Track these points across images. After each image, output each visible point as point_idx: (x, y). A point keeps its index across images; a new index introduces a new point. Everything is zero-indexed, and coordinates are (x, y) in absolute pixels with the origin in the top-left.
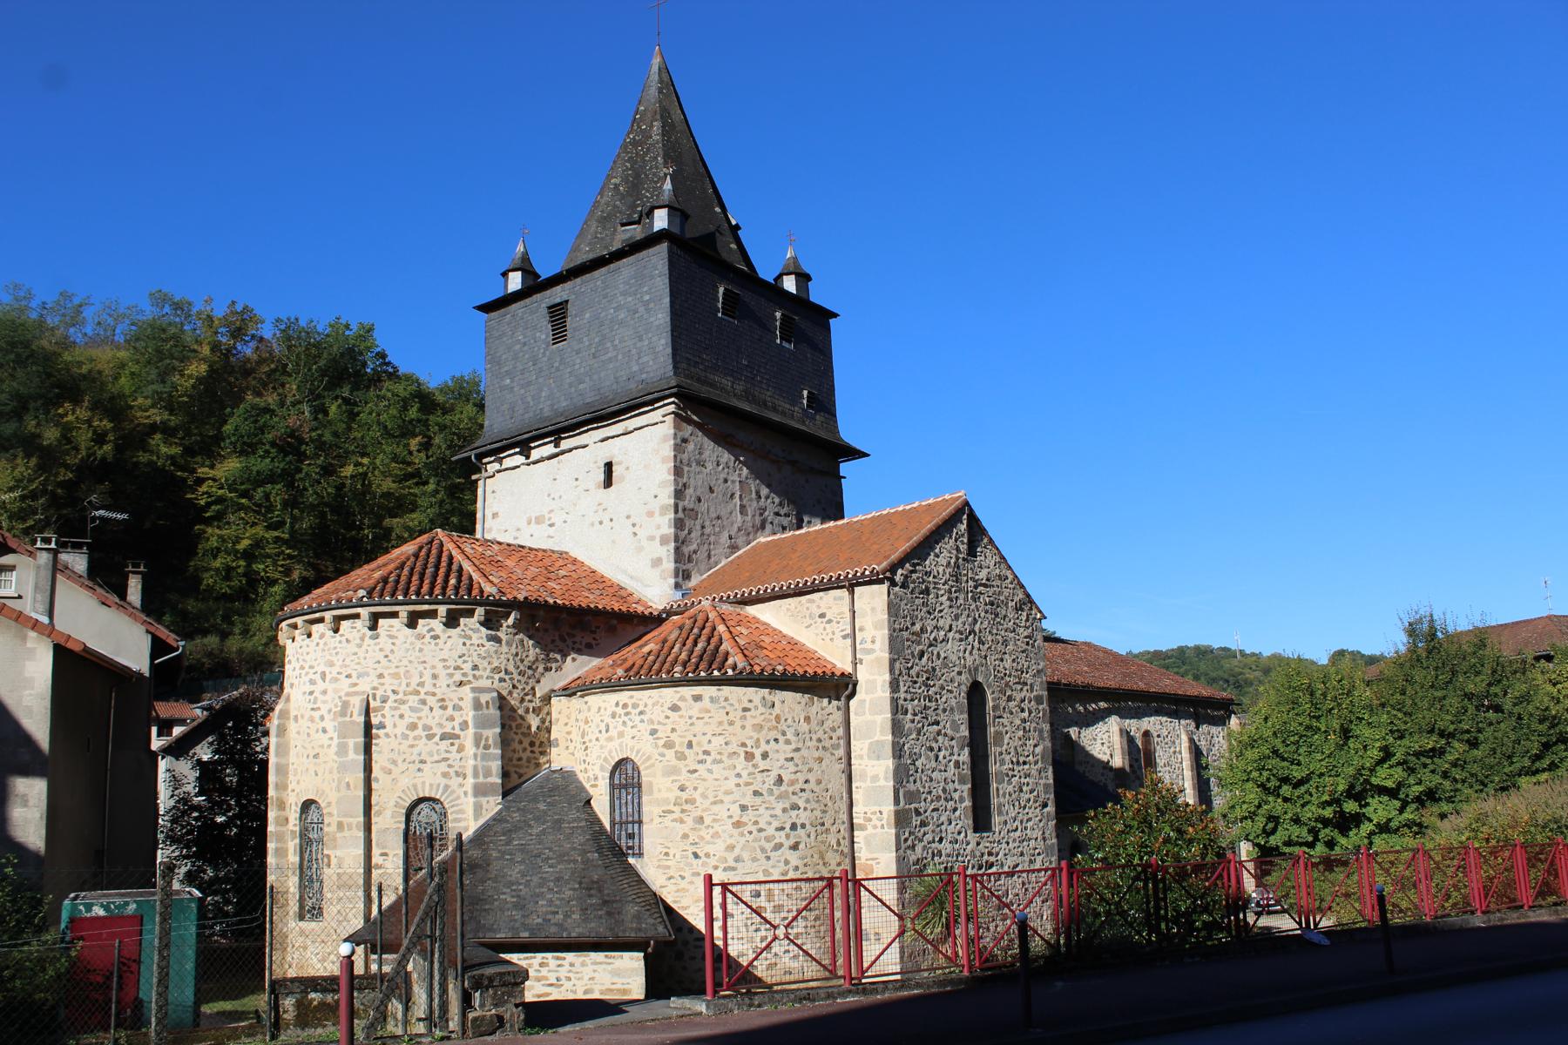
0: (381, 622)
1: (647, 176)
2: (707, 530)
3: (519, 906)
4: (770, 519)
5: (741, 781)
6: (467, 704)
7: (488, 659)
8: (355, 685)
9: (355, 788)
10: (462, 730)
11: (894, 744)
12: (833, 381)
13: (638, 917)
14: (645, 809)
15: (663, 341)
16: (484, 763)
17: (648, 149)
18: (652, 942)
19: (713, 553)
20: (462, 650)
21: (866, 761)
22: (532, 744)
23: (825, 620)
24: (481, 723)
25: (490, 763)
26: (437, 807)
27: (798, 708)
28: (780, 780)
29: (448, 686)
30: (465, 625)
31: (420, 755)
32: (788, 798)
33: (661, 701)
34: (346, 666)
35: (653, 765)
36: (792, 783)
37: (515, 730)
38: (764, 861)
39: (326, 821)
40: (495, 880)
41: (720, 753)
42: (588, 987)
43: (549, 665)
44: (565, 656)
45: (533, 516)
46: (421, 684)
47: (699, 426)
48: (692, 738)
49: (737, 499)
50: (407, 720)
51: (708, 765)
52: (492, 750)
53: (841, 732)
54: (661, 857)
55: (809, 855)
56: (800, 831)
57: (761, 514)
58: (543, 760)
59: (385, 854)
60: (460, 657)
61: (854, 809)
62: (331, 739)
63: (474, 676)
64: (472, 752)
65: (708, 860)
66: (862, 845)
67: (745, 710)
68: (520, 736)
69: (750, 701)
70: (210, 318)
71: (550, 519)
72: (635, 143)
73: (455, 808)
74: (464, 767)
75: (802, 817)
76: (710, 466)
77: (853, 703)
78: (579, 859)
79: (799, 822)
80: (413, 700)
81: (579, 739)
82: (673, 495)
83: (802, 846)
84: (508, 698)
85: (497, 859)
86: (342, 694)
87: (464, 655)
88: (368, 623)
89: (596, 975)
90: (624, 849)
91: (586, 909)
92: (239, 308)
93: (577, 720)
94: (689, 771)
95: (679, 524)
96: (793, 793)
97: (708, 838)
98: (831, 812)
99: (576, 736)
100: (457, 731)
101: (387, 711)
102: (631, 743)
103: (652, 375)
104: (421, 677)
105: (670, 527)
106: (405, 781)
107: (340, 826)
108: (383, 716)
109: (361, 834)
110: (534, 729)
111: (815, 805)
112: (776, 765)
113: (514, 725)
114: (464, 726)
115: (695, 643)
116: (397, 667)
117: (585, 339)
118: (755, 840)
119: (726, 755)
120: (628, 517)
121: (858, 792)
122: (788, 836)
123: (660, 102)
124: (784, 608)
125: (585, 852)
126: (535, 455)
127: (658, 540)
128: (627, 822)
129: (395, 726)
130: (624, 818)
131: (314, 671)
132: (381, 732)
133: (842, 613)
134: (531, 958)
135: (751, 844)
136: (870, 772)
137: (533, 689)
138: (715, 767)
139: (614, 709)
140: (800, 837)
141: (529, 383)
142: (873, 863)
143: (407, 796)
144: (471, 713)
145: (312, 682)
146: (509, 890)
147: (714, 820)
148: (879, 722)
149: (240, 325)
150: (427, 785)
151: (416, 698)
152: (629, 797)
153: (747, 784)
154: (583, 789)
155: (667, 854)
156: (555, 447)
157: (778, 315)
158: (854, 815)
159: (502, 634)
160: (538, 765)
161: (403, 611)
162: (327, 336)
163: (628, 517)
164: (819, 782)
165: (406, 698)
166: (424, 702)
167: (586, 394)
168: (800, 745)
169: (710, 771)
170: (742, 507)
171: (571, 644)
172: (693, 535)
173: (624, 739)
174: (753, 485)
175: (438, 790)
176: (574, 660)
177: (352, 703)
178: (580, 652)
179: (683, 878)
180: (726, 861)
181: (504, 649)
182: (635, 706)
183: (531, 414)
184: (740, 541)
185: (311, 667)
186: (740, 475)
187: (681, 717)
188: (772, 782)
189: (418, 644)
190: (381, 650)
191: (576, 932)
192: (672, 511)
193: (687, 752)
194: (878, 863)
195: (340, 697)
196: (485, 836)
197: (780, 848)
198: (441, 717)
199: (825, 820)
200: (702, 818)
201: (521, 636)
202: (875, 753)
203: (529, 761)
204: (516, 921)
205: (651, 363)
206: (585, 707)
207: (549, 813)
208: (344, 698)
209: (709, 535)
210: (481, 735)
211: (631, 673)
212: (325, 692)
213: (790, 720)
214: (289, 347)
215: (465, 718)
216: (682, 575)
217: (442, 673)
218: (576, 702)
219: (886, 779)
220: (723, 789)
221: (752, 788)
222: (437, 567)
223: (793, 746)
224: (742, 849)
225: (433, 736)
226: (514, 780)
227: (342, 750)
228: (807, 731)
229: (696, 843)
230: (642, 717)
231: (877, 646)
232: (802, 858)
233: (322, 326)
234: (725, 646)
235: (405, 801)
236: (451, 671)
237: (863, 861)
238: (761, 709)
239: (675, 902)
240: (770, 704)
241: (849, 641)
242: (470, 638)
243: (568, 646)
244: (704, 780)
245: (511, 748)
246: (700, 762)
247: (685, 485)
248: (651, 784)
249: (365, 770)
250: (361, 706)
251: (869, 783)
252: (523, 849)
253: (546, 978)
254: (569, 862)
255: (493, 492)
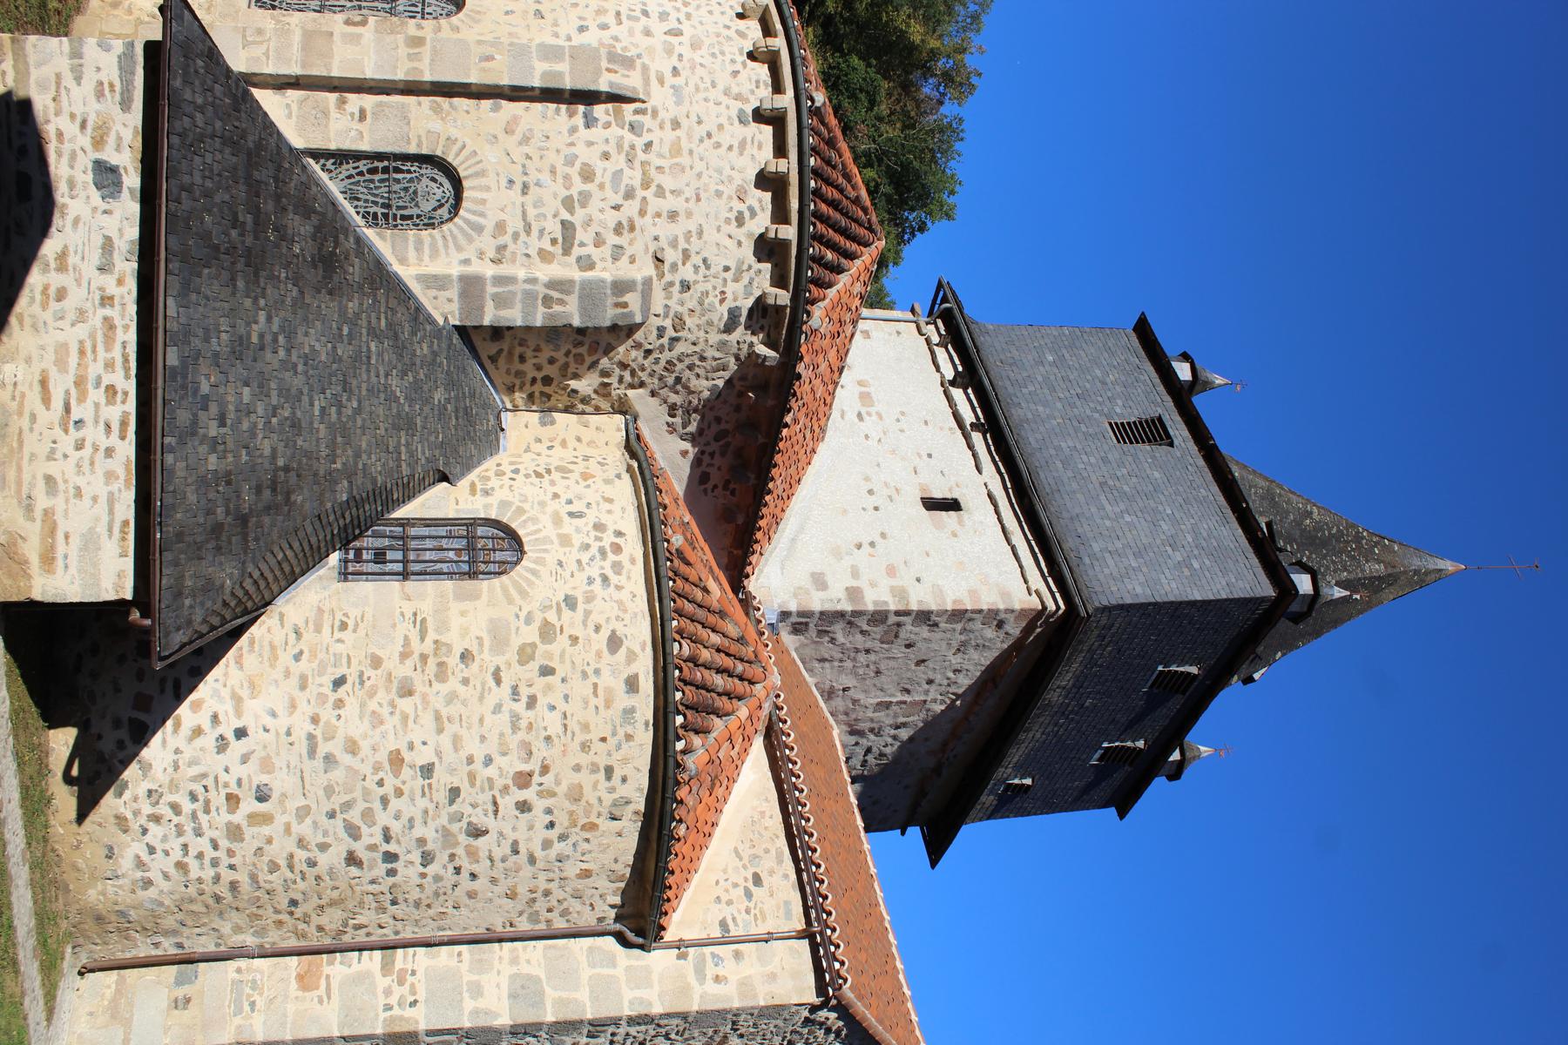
0: (768, 130)
1: (1324, 557)
2: (862, 658)
3: (240, 349)
4: (863, 742)
5: (478, 765)
6: (624, 270)
7: (698, 309)
8: (661, 82)
9: (483, 70)
10: (579, 259)
11: (538, 1026)
12: (1035, 814)
13: (209, 587)
14: (430, 587)
15: (1139, 590)
16: (519, 296)
17: (1353, 558)
18: (148, 622)
19: (827, 665)
20: (717, 263)
21: (508, 970)
22: (547, 381)
23: (750, 885)
24: (590, 294)
25: (519, 306)
26: (444, 212)
27: (607, 859)
28: (477, 832)
29: (656, 239)
30: (760, 271)
31: (538, 184)
32: (444, 848)
33: (627, 617)
34: (693, 68)
35: (510, 601)
36: (472, 854)
37: (574, 351)
38: (327, 807)
39: (424, 23)
40: (299, 303)
41: (530, 726)
42: (61, 486)
43: (680, 412)
44: (693, 439)
45: (871, 390)
46: (660, 192)
47: (1018, 645)
48: (560, 673)
49: (900, 697)
50: (599, 166)
51: (510, 705)
52: (541, 310)
53: (560, 924)
54: (339, 616)
55: (337, 884)
56: (382, 868)
57: (872, 730)
58: (519, 397)
59: (362, 115)
60: (705, 261)
61: (421, 951)
62: (569, 39)
63: (671, 284)
64: (538, 274)
65: (330, 704)
66: (356, 967)
67: (609, 771)
68: (562, 360)
69: (624, 780)
70: (964, 50)
71: (869, 414)
72: (1358, 538)
73: (440, 242)
74: (514, 261)
75: (409, 871)
76: (956, 660)
77: (610, 941)
78: (338, 466)
79: (398, 865)
80: (633, 177)
81: (555, 462)
82: (924, 608)
83: (354, 871)
84: (630, 342)
85: (343, 312)
86: (646, 60)
87: (708, 267)
88: (767, 105)
89: (87, 501)
90: (357, 544)
91: (229, 483)
92: (974, 80)
93: (586, 458)
94: (498, 670)
95: (879, 617)
96: (452, 857)
97: (373, 705)
98: (416, 914)
99: (558, 456)
100: (577, 251)
101: (615, 131)
102: (551, 560)
103: (1091, 572)
104: (673, 192)
105: (875, 603)
106: (491, 156)
107: (418, 42)
108: (607, 125)
109: (400, 75)
110: (573, 384)
111: (429, 890)
112: (507, 825)
113: (583, 350)
114: (586, 263)
115: (719, 671)
116: (691, 152)
117: (1124, 471)
118: (366, 793)
119: (528, 738)
120: (883, 535)
121: (450, 955)
122: (372, 848)
123: (1405, 572)
124: (764, 806)
125: (350, 474)
126: (957, 393)
127: (855, 584)
128: (405, 550)
129: (590, 144)
130: (413, 544)
131: (683, 18)
132: (579, 120)
133: (764, 919)
134: (127, 370)
135: (360, 784)
136: (487, 981)
137: (642, 385)
138: (505, 717)
139: (611, 529)
140: (371, 868)
141: (1053, 390)
142: (322, 990)
143: (467, 159)
144: (608, 276)
145: (663, 16)
146: (275, 328)
147: (405, 718)
148: (577, 995)
149: (958, 82)
150: (484, 195)
151: (637, 183)
152: (451, 554)
153: (472, 777)
154: (468, 467)
155: (344, 626)
156: (972, 425)
157: (1141, 744)
158: (411, 950)
159: (740, 333)
160: (511, 390)
161: (788, 166)
162: (944, 171)
163: (883, 535)
164: (471, 895)
165: (637, 164)
166: (629, 195)
167: (1048, 475)
168: (540, 864)
169: (497, 709)
170: (888, 705)
171: (709, 449)
172: (859, 637)
173: (556, 545)
174: (917, 720)
175: (474, 213)
176: (684, 453)
177: (631, 73)
178: (697, 462)
179: (298, 657)
180: (327, 739)
181: (715, 338)
182: (617, 568)
183: (1010, 389)
184: (839, 703)
185: (688, 16)
186: (935, 701)
187: (599, 654)
188: (474, 820)
189: (729, 190)
190: (720, 127)
191: (173, 462)
192: (901, 607)
193: (534, 666)
194: (321, 1002)
195: (639, 56)
196: (388, 291)
197: (350, 835)
198: (602, 224)
199: (403, 906)
200: (410, 693)
201: (733, 366)
202: (524, 989)
203: (519, 374)
204: (207, 340)
205: (1106, 571)
206: (611, 474)
207: (427, 409)
208: (638, 62)
209: (854, 660)
210: (568, 293)
211: (677, 562)
212: (648, 33)
213: (586, 846)
214: (932, 131)
215: (599, 265)
216: (799, 622)
217: (678, 229)
218: (617, 458)
219: (476, 1012)
220: (463, 732)
221: (465, 787)
222: (844, 232)
223: (539, 854)
224: (349, 768)
225: (571, 210)
226: (487, 348)
227: (551, 53)
228: (564, 875)
229: (362, 683)
230: (599, 580)
231: (711, 988)
232: (331, 872)
233: (955, 167)
234: (718, 723)
235: (457, 155)
236: (682, 244)
237: (327, 970)
238: (608, 799)
239: (252, 642)
240: (617, 813)
241: (716, 933)
242: (736, 280)
243: (707, 444)
244: (481, 698)
245: (543, 345)
246: (515, 691)
247: (936, 625)
248: (475, 596)
249: (515, 88)
250: (626, 87)
251: (468, 977)
252: (360, 358)
253: (82, 398)
254: (332, 445)
255: (898, 333)
